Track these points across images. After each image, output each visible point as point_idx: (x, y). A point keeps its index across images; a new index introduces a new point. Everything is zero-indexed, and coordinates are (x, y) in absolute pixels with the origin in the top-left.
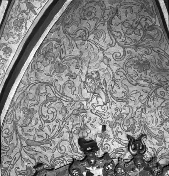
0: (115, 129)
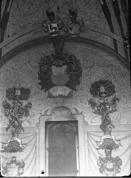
0: (63, 9)
